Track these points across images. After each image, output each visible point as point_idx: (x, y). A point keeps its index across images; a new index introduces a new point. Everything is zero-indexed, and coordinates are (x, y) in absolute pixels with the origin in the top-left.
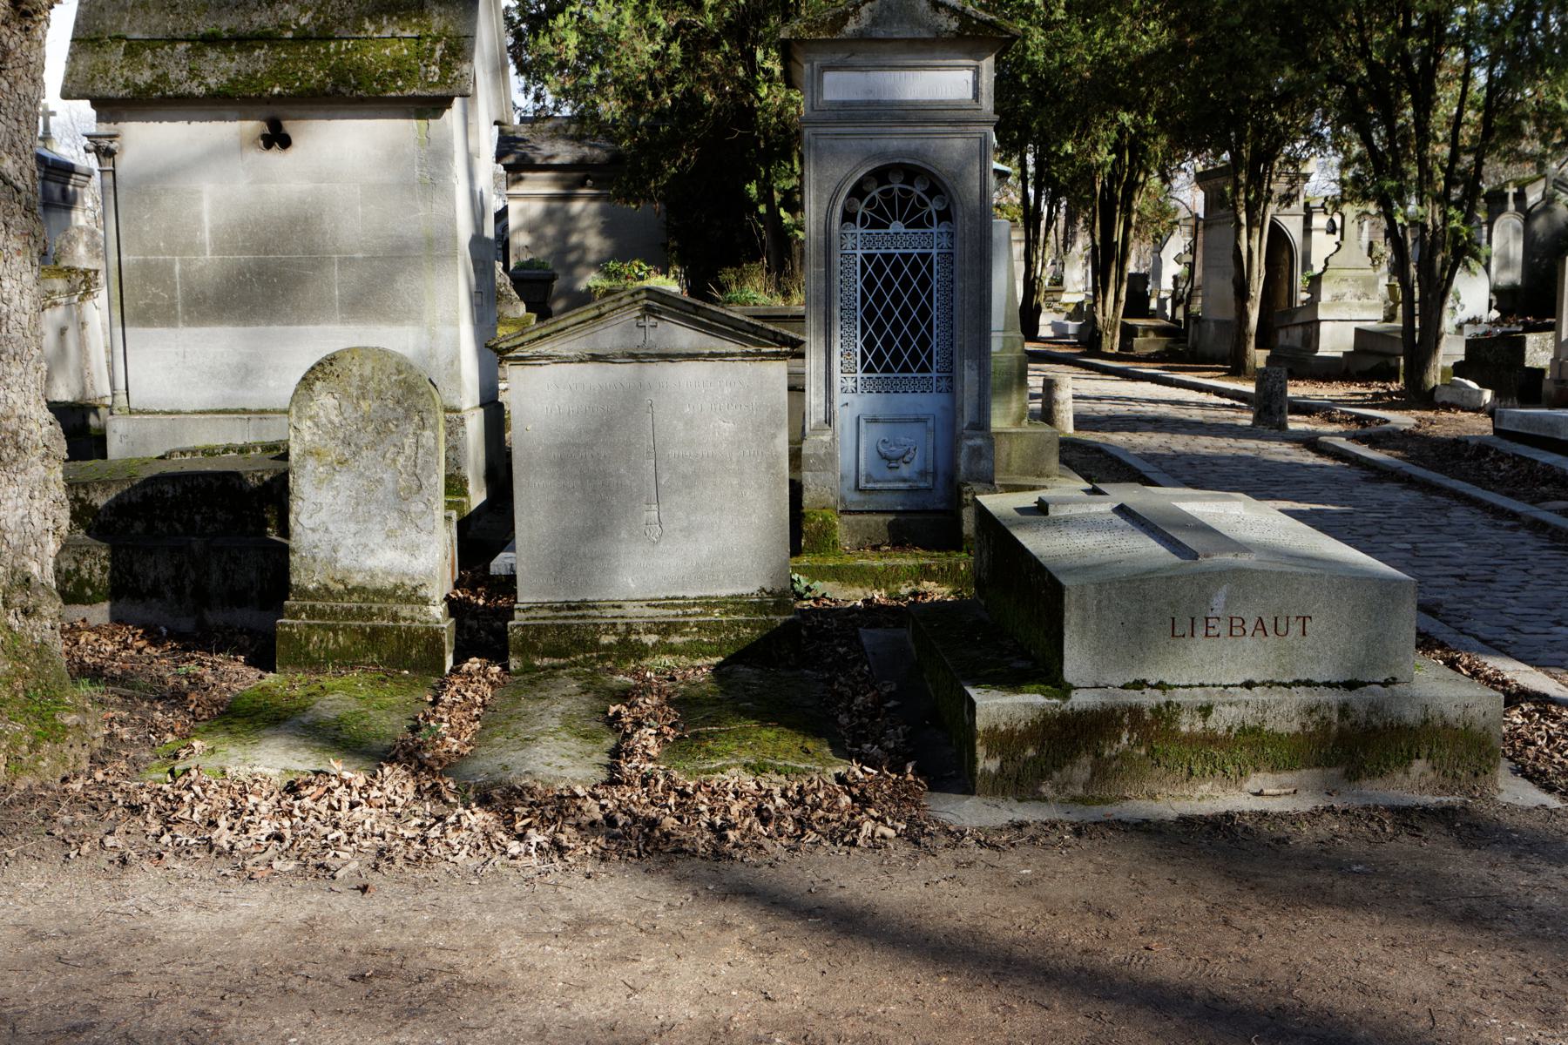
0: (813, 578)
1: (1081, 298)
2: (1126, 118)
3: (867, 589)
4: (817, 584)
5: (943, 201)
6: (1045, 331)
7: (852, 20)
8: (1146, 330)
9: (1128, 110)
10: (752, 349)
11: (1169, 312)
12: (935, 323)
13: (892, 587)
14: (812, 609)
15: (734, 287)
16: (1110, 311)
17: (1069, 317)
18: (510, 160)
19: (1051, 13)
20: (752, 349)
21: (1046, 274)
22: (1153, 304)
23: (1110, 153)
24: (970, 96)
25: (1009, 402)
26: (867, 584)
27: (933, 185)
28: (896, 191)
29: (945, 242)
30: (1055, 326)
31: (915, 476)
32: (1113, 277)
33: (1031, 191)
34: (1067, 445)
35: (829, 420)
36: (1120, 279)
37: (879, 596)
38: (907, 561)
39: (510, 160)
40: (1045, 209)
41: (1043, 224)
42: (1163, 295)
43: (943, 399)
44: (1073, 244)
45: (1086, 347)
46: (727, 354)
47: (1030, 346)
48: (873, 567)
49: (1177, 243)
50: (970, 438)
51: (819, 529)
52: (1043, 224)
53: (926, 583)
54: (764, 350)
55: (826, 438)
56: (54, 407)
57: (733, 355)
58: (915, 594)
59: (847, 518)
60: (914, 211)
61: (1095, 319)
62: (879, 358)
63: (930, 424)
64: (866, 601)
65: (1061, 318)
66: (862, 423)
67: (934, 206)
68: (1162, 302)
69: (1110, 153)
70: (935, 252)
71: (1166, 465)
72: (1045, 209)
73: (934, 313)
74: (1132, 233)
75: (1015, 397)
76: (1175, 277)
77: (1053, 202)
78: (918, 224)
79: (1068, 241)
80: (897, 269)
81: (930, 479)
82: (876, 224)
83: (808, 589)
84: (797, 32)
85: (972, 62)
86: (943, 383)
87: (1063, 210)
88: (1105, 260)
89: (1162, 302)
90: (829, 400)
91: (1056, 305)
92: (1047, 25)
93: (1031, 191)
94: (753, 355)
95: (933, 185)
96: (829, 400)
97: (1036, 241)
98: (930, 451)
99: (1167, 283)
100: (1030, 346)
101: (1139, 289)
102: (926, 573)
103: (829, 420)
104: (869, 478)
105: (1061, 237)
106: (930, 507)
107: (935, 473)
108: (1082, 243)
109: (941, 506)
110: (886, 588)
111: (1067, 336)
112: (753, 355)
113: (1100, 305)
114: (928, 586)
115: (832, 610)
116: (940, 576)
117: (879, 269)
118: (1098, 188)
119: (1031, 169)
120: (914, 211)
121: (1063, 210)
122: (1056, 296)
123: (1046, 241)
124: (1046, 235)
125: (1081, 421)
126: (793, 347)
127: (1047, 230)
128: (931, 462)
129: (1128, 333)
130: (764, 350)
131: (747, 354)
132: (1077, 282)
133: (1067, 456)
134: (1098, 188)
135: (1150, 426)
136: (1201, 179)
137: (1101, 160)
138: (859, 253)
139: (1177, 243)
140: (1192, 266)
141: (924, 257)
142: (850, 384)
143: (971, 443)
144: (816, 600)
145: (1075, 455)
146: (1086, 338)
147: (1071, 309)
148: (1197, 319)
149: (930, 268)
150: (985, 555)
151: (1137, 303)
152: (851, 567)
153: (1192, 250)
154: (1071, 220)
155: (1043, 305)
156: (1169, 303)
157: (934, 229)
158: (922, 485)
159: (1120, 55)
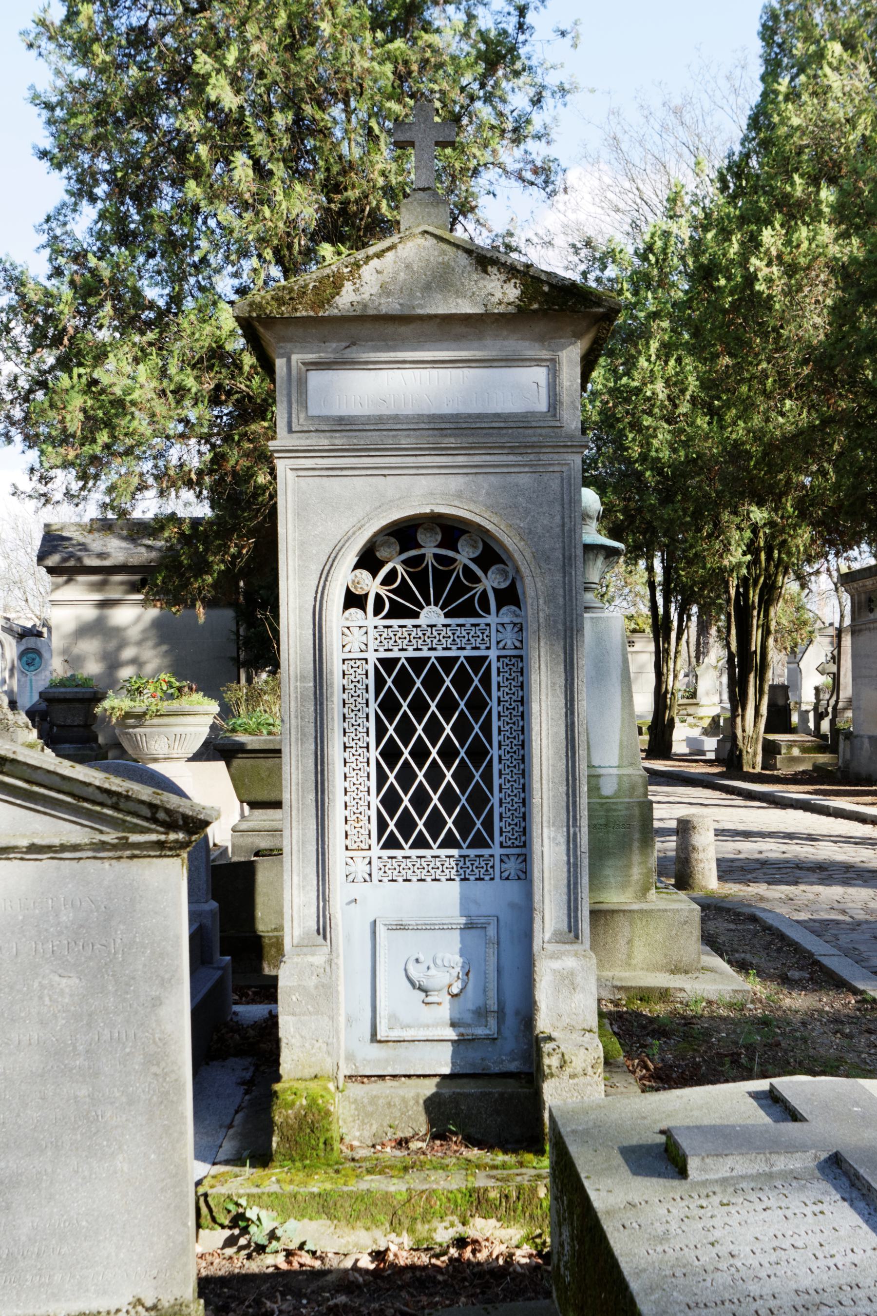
0: (285, 1214)
1: (716, 711)
2: (758, 515)
3: (378, 1233)
4: (292, 1224)
5: (505, 574)
6: (679, 747)
7: (348, 286)
8: (791, 745)
9: (760, 504)
10: (111, 836)
11: (811, 725)
12: (496, 767)
13: (422, 1229)
14: (278, 1273)
15: (243, 710)
16: (752, 726)
17: (706, 732)
18: (53, 560)
19: (676, 406)
20: (111, 836)
21: (677, 684)
22: (795, 718)
23: (744, 554)
24: (543, 406)
25: (629, 866)
26: (376, 1223)
27: (487, 548)
28: (430, 560)
29: (509, 638)
30: (690, 741)
31: (468, 1017)
32: (751, 691)
33: (660, 601)
34: (713, 909)
35: (323, 930)
36: (760, 692)
37: (401, 1249)
38: (449, 1182)
39: (53, 560)
40: (674, 616)
41: (673, 635)
42: (804, 707)
43: (512, 889)
44: (706, 654)
45: (728, 769)
46: (63, 848)
47: (660, 765)
48: (387, 1195)
49: (817, 653)
50: (553, 956)
51: (301, 1120)
52: (673, 635)
53: (478, 1222)
54: (134, 838)
55: (319, 959)
56: (198, 757)
57: (75, 848)
58: (461, 1242)
59: (356, 1090)
60: (441, 578)
61: (735, 736)
62: (406, 825)
63: (492, 931)
64: (379, 1255)
65: (696, 733)
66: (381, 930)
67: (491, 582)
68: (804, 715)
69: (744, 554)
70: (493, 654)
71: (844, 939)
72: (674, 616)
73: (495, 752)
74: (771, 641)
75: (636, 858)
76: (817, 689)
77: (683, 611)
78: (466, 610)
79: (700, 652)
80: (433, 683)
81: (492, 1022)
82: (397, 611)
83: (273, 1236)
84: (260, 306)
85: (545, 354)
86: (512, 866)
87: (694, 619)
88: (744, 668)
89: (804, 715)
90: (323, 896)
91: (690, 719)
92: (670, 420)
93: (660, 601)
94: (114, 847)
95: (487, 548)
96: (323, 896)
97: (667, 651)
98: (493, 975)
99: (808, 697)
100: (660, 765)
101: (781, 702)
102: (479, 1203)
103: (323, 930)
104: (394, 1019)
105: (693, 648)
106: (496, 1069)
107: (501, 1013)
108: (716, 654)
109: (513, 1067)
110: (411, 1230)
111: (703, 753)
112: (114, 847)
113: (739, 720)
114: (481, 1227)
115: (315, 1274)
116: (506, 1207)
117: (404, 682)
118: (733, 592)
119: (659, 578)
120: (441, 578)
121: (694, 619)
122: (691, 710)
123: (676, 652)
124: (677, 644)
125: (729, 870)
126: (190, 833)
127: (679, 639)
128: (493, 994)
129: (771, 750)
130: (134, 838)
131: (103, 846)
132: (713, 695)
133: (711, 926)
134: (733, 592)
135: (814, 877)
136: (847, 580)
137: (734, 560)
138: (372, 657)
139: (817, 653)
140: (836, 678)
141: (477, 662)
142: (361, 868)
143: (556, 965)
144: (289, 1254)
145: (721, 926)
146: (725, 755)
147: (706, 723)
148: (849, 735)
149: (486, 680)
150: (566, 1233)
151: (779, 718)
152: (349, 1195)
153: (836, 659)
154: (703, 629)
155: (677, 720)
156: (811, 715)
157: (492, 619)
158: (480, 1031)
159: (755, 439)
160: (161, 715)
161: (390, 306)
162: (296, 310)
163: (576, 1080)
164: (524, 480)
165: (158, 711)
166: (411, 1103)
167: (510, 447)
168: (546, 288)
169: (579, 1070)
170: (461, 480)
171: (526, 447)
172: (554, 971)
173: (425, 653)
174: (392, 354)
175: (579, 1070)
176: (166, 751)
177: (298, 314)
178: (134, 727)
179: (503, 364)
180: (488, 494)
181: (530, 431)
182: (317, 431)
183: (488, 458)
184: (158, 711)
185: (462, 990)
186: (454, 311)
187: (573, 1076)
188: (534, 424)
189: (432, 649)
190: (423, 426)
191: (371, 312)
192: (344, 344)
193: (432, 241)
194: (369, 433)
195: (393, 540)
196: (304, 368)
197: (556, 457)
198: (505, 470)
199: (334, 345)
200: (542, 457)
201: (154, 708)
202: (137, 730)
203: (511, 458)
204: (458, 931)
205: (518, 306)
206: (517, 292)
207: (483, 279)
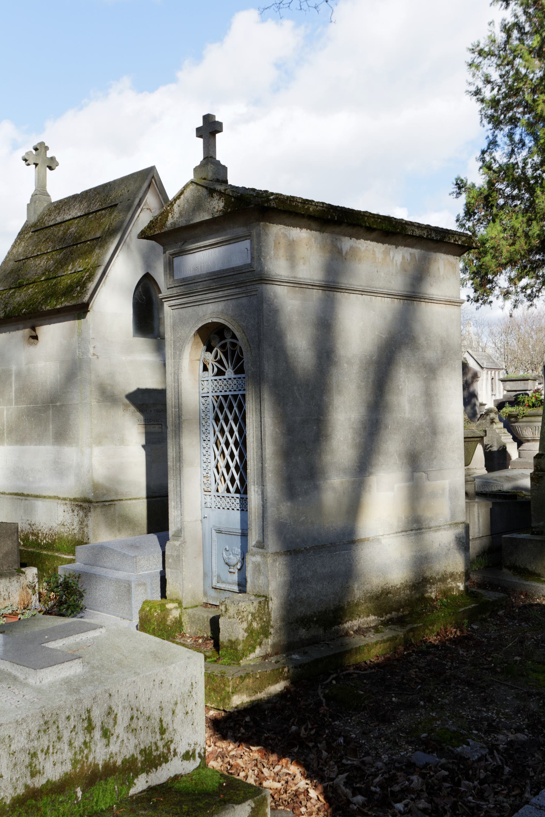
160: (525, 416)
161: (183, 223)
162: (155, 231)
163: (231, 620)
164: (244, 301)
165: (524, 413)
166: (206, 620)
167: (235, 284)
168: (233, 200)
169: (232, 615)
170: (223, 303)
171: (240, 283)
172: (253, 563)
173: (227, 393)
174: (196, 244)
175: (232, 615)
176: (532, 436)
177: (156, 233)
178: (514, 422)
179: (234, 241)
180: (232, 310)
181: (243, 275)
182: (175, 287)
183: (229, 291)
184: (524, 413)
185: (241, 567)
186: (202, 219)
187: (229, 618)
188: (244, 271)
189: (230, 391)
190: (207, 279)
191: (177, 227)
192: (182, 243)
193: (195, 185)
194: (191, 285)
195: (216, 336)
196: (171, 257)
197: (252, 287)
198: (237, 297)
199: (180, 244)
200: (248, 288)
201: (521, 412)
202: (516, 424)
203: (237, 290)
204: (240, 537)
205: (223, 211)
206: (222, 204)
207: (212, 200)
